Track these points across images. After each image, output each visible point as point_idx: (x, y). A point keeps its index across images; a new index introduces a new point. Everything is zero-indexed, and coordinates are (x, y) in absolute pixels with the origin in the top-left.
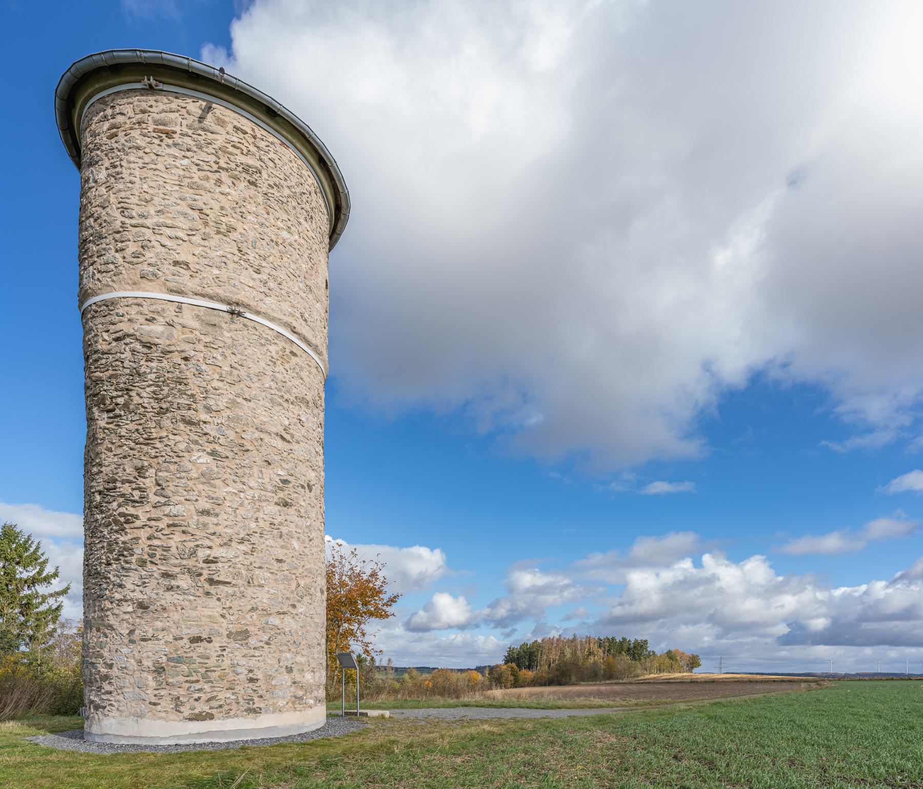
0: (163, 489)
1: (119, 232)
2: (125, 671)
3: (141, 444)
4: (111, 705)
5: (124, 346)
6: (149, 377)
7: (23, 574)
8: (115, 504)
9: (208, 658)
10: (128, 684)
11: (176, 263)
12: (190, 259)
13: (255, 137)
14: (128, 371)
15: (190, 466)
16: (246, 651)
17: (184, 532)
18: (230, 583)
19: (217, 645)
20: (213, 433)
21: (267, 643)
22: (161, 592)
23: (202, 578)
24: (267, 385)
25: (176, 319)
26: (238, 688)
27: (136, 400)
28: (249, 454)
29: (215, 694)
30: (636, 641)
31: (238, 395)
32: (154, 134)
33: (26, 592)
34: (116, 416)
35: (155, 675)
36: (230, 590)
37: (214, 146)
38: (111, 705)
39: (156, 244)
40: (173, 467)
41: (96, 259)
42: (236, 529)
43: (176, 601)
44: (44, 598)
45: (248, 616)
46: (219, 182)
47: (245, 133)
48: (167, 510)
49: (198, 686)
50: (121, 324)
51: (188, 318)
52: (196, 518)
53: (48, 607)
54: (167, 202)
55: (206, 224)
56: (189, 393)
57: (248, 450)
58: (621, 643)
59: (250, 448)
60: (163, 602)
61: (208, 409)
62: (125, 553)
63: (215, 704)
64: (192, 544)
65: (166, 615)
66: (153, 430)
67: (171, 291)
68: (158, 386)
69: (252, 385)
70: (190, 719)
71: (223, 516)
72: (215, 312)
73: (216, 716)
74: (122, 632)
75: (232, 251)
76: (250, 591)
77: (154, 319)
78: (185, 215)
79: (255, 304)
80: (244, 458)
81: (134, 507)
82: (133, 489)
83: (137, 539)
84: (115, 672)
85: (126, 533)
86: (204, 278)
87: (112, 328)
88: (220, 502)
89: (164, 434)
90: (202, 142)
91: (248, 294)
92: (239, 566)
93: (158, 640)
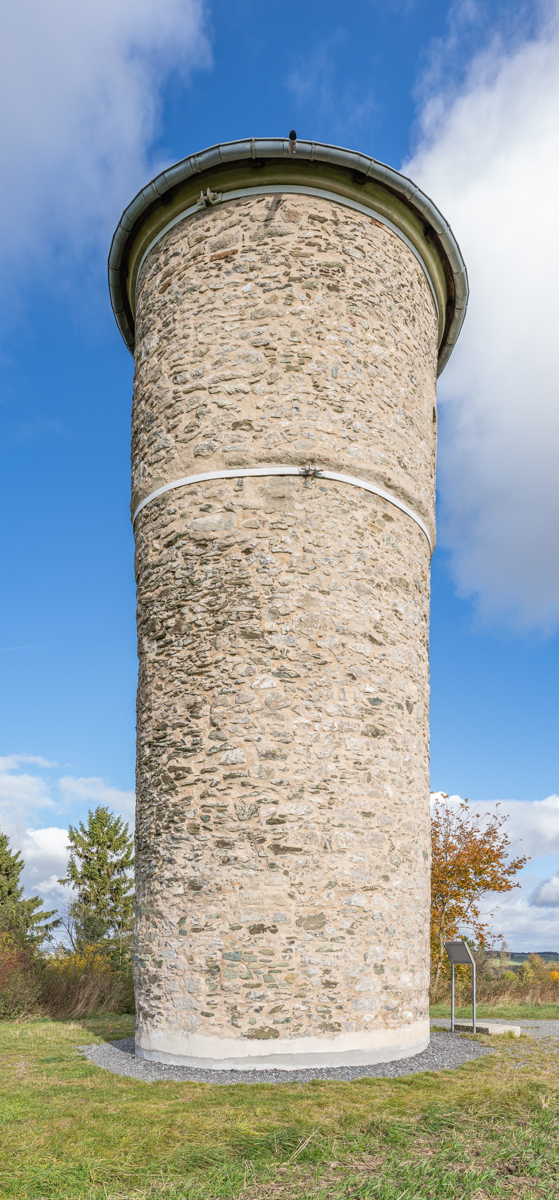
0: (219, 730)
1: (170, 406)
2: (175, 971)
3: (194, 674)
4: (159, 1013)
5: (175, 551)
8: (165, 757)
9: (272, 954)
11: (236, 425)
15: (251, 694)
16: (321, 944)
17: (243, 784)
21: (350, 932)
22: (215, 866)
23: (265, 845)
25: (235, 501)
26: (310, 995)
27: (189, 617)
28: (327, 667)
29: (280, 1003)
35: (208, 976)
36: (300, 859)
38: (159, 1013)
40: (230, 699)
42: (309, 775)
43: (233, 878)
45: (324, 895)
48: (223, 756)
49: (259, 992)
50: (172, 524)
52: (258, 763)
57: (325, 663)
59: (328, 659)
60: (218, 880)
61: (275, 613)
62: (176, 818)
64: (253, 800)
65: (221, 897)
66: (208, 654)
67: (230, 464)
68: (214, 594)
69: (331, 571)
70: (250, 1037)
73: (281, 1033)
74: (172, 920)
75: (306, 389)
76: (326, 860)
77: (210, 506)
78: (246, 358)
79: (336, 455)
80: (320, 674)
81: (185, 757)
82: (185, 735)
83: (188, 799)
84: (164, 972)
86: (270, 436)
88: (289, 739)
89: (220, 656)
93: (212, 930)
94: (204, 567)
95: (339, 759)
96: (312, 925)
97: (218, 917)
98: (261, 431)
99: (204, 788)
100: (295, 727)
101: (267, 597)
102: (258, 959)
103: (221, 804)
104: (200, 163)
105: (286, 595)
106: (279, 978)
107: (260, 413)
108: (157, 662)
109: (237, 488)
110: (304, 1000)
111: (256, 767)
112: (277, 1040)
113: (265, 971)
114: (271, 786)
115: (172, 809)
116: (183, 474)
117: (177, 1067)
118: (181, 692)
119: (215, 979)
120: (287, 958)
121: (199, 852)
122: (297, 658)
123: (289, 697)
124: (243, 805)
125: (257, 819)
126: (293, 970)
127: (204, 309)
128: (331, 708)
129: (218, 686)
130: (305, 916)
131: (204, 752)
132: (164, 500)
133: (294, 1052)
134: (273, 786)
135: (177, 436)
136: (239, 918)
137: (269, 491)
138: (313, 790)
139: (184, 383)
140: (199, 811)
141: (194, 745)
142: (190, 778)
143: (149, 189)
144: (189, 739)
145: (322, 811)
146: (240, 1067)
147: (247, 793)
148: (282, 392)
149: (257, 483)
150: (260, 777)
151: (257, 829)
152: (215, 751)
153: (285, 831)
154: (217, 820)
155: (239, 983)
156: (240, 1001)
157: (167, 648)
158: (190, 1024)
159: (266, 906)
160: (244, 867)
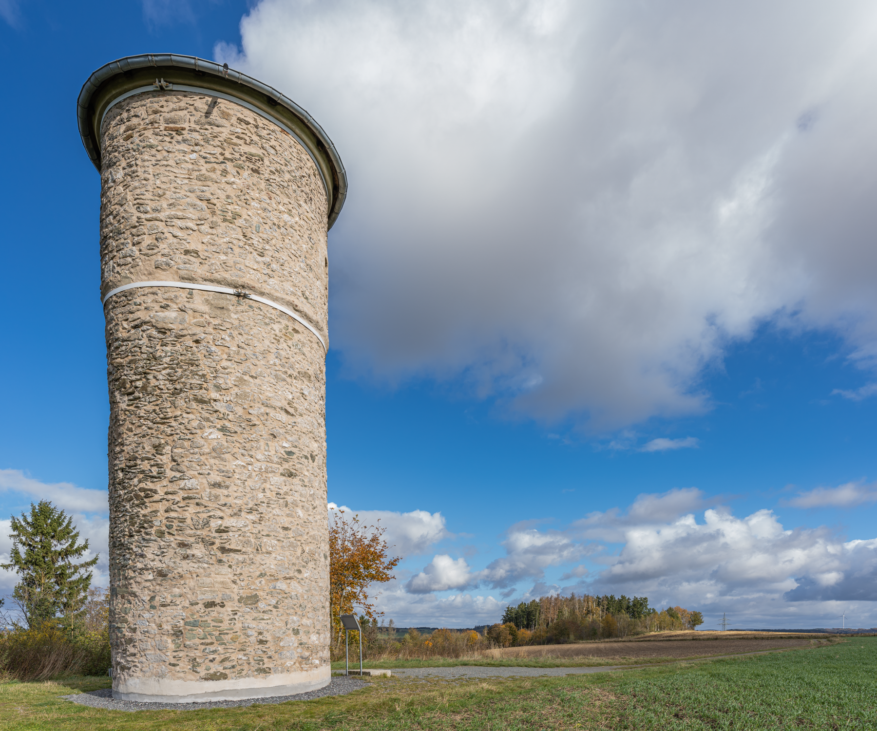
0: (178, 464)
1: (135, 227)
3: (158, 423)
4: (135, 666)
6: (164, 360)
7: (58, 546)
8: (136, 480)
9: (221, 622)
10: (150, 647)
11: (187, 252)
12: (199, 247)
13: (257, 127)
14: (145, 356)
15: (202, 442)
16: (256, 615)
17: (197, 504)
20: (222, 410)
21: (275, 607)
23: (215, 547)
25: (187, 305)
26: (249, 649)
27: (153, 382)
28: (256, 428)
29: (228, 655)
30: (636, 598)
32: (165, 133)
33: (60, 563)
34: (135, 399)
35: (174, 638)
36: (240, 557)
37: (220, 139)
38: (135, 666)
40: (187, 444)
42: (245, 500)
43: (191, 569)
44: (76, 568)
45: (257, 582)
46: (225, 172)
47: (248, 123)
48: (182, 484)
49: (212, 648)
51: (198, 303)
52: (208, 490)
54: (178, 195)
55: (213, 213)
56: (200, 373)
57: (255, 425)
58: (620, 601)
59: (257, 423)
60: (180, 570)
61: (218, 388)
62: (146, 525)
63: (228, 664)
64: (205, 515)
65: (182, 582)
66: (168, 410)
67: (183, 279)
68: (172, 368)
69: (258, 363)
70: (206, 679)
72: (223, 295)
74: (144, 598)
75: (237, 237)
76: (258, 558)
77: (168, 306)
78: (194, 206)
79: (260, 285)
81: (152, 482)
83: (156, 512)
84: (138, 636)
86: (212, 264)
87: (131, 316)
88: (230, 475)
89: (178, 413)
90: (209, 136)
91: (253, 277)
92: (248, 534)
106: (227, 638)
113: (217, 633)
128: (260, 456)
136: (197, 597)
140: (164, 521)
144: (155, 470)
146: (199, 700)
160: (199, 562)
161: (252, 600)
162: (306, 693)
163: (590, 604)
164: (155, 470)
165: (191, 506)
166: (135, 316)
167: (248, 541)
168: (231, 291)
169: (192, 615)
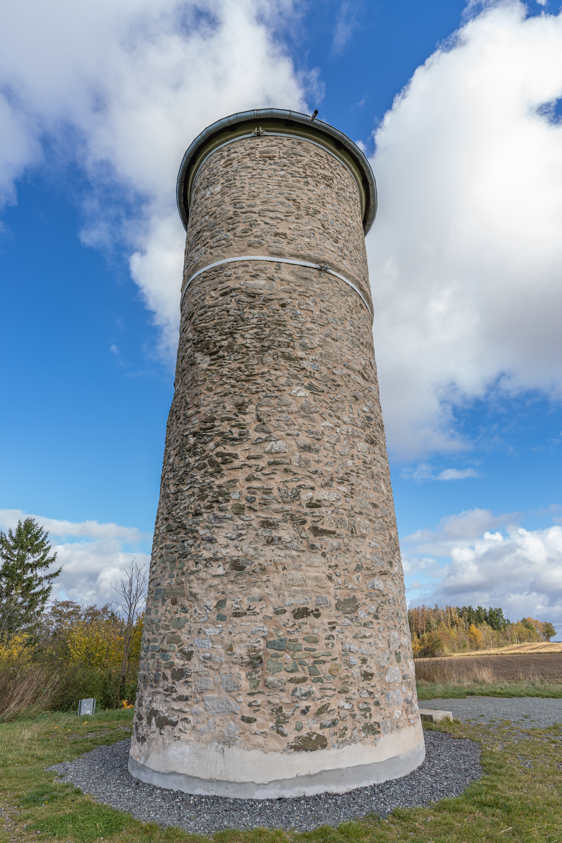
0: (264, 424)
1: (231, 218)
2: (209, 663)
3: (242, 381)
4: (185, 719)
5: (230, 299)
6: (252, 321)
7: (31, 559)
8: (211, 445)
9: (316, 642)
10: (211, 686)
11: (276, 234)
12: (287, 231)
13: (328, 160)
14: (233, 318)
15: (290, 400)
16: (356, 630)
17: (286, 470)
18: (334, 533)
19: (326, 621)
20: (309, 368)
21: (376, 617)
22: (259, 546)
23: (306, 527)
24: (348, 329)
25: (275, 275)
26: (353, 689)
27: (240, 341)
28: (341, 388)
29: (326, 700)
30: (491, 609)
31: (327, 336)
32: (260, 159)
33: (29, 575)
34: (220, 357)
35: (249, 670)
36: (335, 542)
37: (302, 163)
38: (185, 719)
39: (261, 223)
40: (274, 402)
41: (209, 241)
42: (336, 467)
43: (277, 558)
44: (41, 580)
45: (354, 577)
46: (307, 183)
47: (322, 157)
48: (268, 446)
49: (304, 688)
50: (228, 282)
51: (285, 274)
52: (297, 454)
53: (41, 588)
54: (270, 196)
55: (298, 208)
56: (287, 332)
57: (339, 385)
58: (478, 612)
59: (341, 383)
60: (262, 560)
61: (304, 347)
62: (220, 498)
63: (327, 718)
64: (294, 485)
65: (265, 578)
66: (255, 367)
67: (272, 254)
68: (260, 328)
69: (338, 327)
70: (297, 748)
71: (323, 452)
72: (307, 269)
73: (331, 740)
74: (208, 604)
75: (318, 226)
76: (353, 543)
77: (258, 275)
78: (282, 203)
79: (337, 263)
80: (336, 392)
81: (233, 445)
82: (232, 426)
83: (235, 481)
84: (195, 665)
85: (222, 476)
86: (298, 244)
87: (220, 286)
88: (320, 437)
89: (266, 370)
90: (294, 161)
91: (331, 256)
92: (341, 510)
93: (255, 614)
94: (252, 311)
95: (354, 458)
96: (348, 609)
97: (260, 600)
98: (293, 240)
99: (249, 472)
100: (322, 428)
101: (298, 335)
102: (303, 647)
103: (266, 487)
104: (259, 114)
105: (312, 336)
106: (324, 669)
107: (291, 232)
108: (209, 370)
109: (277, 268)
110: (347, 695)
111: (297, 457)
112: (325, 751)
113: (310, 661)
114: (308, 474)
115: (217, 490)
116: (238, 255)
117: (207, 797)
118: (230, 393)
119: (257, 672)
120: (330, 646)
121: (243, 532)
122: (321, 379)
123: (317, 405)
124: (285, 489)
125: (298, 503)
126: (336, 659)
127: (256, 177)
128: (346, 418)
129: (263, 391)
130: (342, 599)
131: (249, 442)
132: (222, 268)
133: (343, 766)
134: (310, 474)
135: (235, 234)
136: (284, 601)
137: (297, 273)
138: (339, 481)
139: (241, 208)
140: (245, 493)
141: (240, 435)
142: (237, 463)
143: (226, 120)
144: (236, 431)
145: (347, 499)
146: (288, 794)
147: (289, 479)
148: (304, 224)
149: (290, 268)
150: (300, 466)
151: (299, 512)
152: (261, 441)
153: (322, 514)
154: (262, 502)
155: (284, 678)
156: (286, 700)
157: (219, 361)
158: (227, 735)
159: (309, 589)
160: (287, 548)
161: (349, 605)
162: (419, 768)
163: (453, 615)
164: (236, 432)
165: (278, 473)
166: (225, 285)
167: (342, 519)
168: (314, 265)
169: (277, 630)
